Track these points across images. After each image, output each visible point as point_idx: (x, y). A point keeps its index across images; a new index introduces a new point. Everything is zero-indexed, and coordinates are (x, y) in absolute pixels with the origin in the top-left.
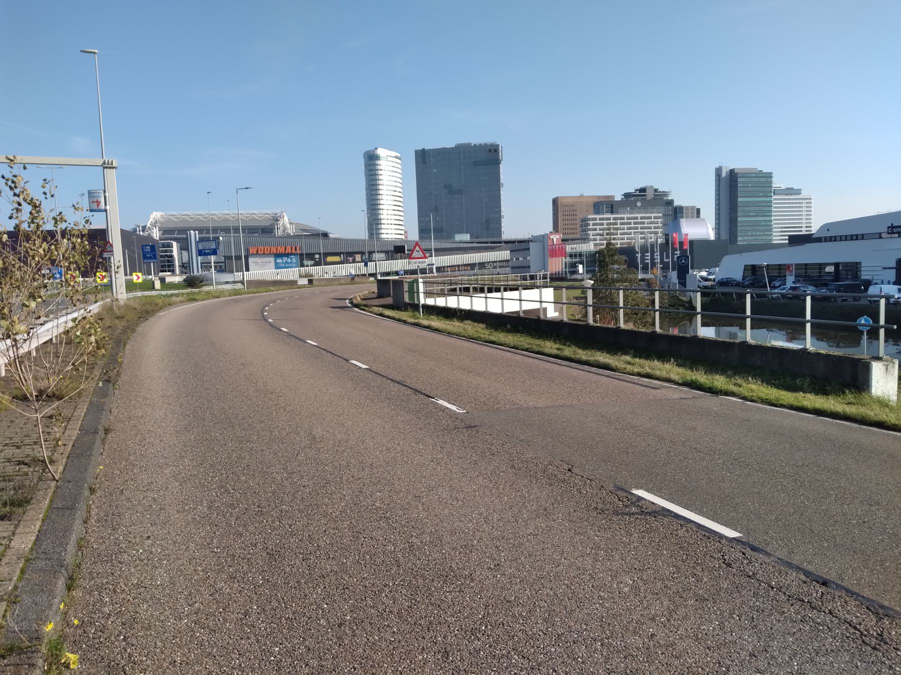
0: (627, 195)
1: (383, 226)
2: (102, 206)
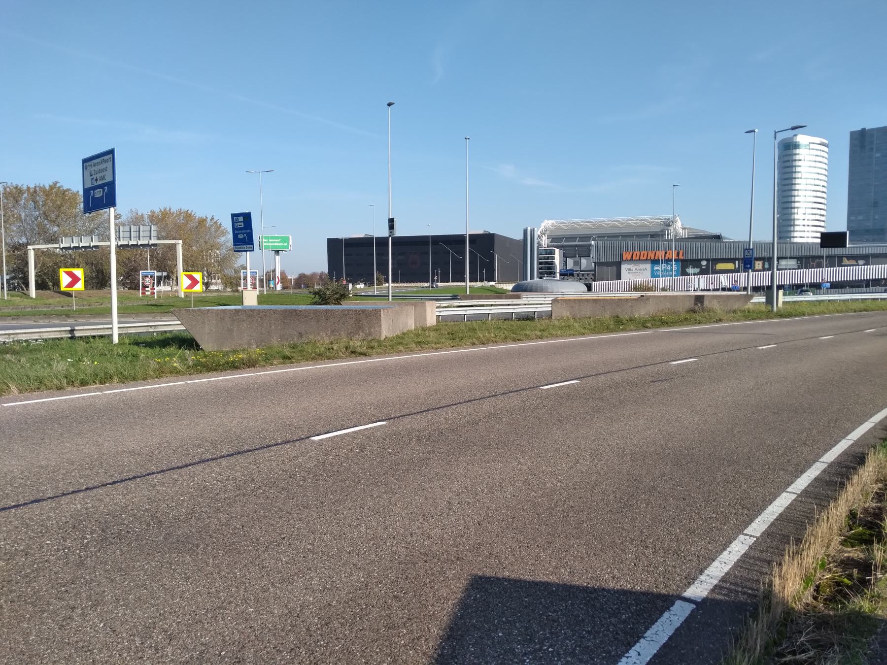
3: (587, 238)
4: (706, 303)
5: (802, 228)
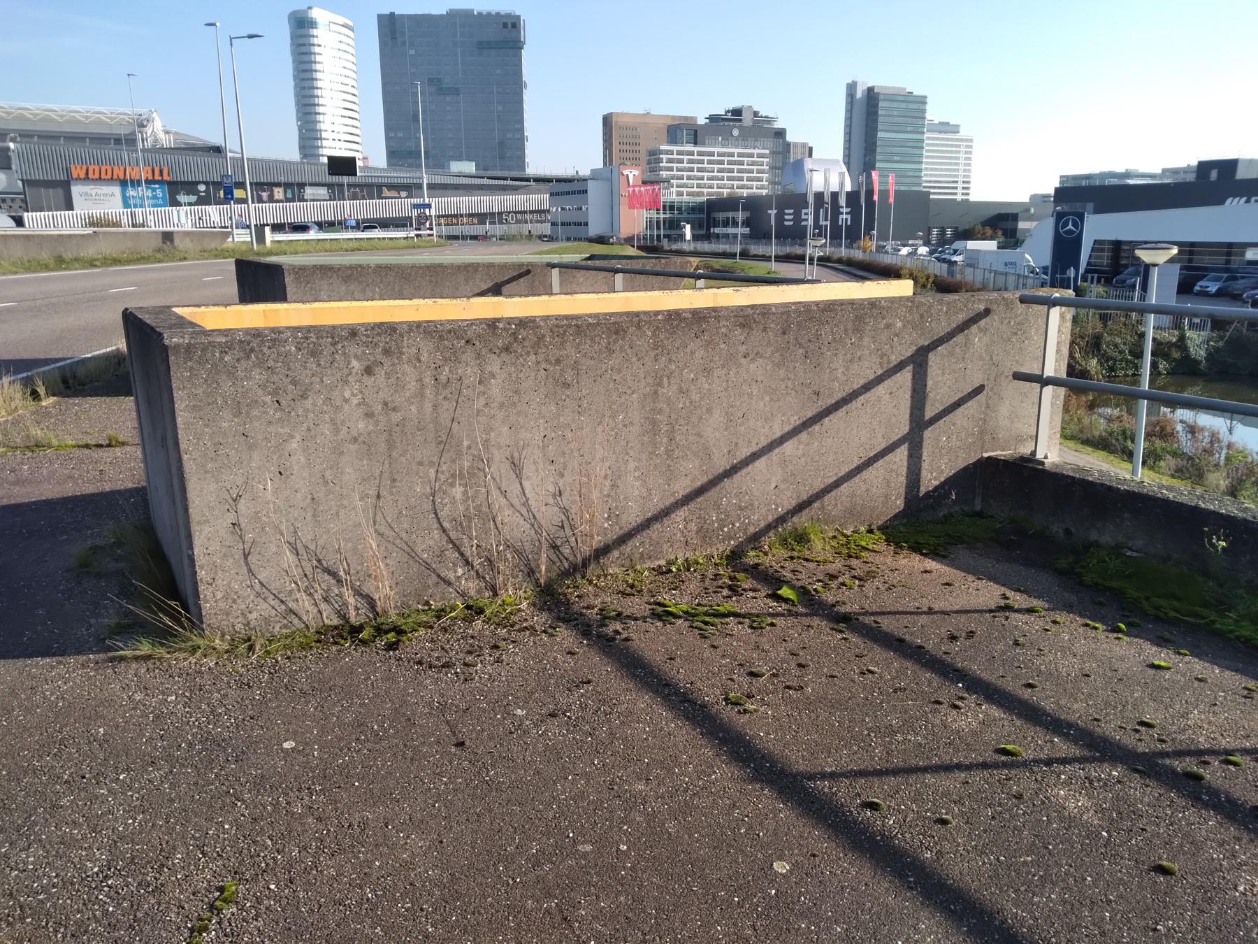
0: (713, 119)
1: (325, 143)
4: (177, 241)
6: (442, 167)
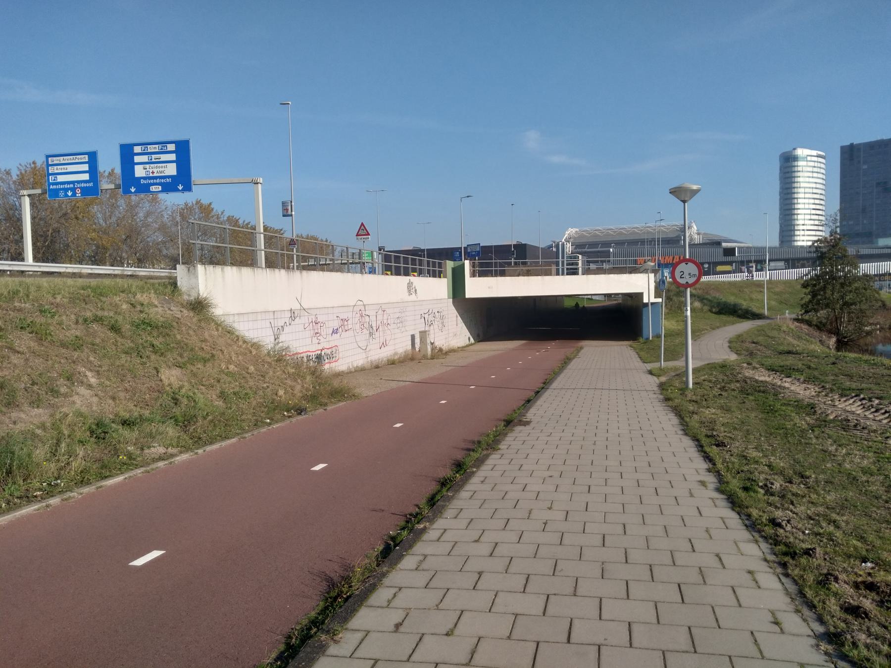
2: (289, 212)
3: (607, 244)
5: (802, 233)
6: (871, 242)
